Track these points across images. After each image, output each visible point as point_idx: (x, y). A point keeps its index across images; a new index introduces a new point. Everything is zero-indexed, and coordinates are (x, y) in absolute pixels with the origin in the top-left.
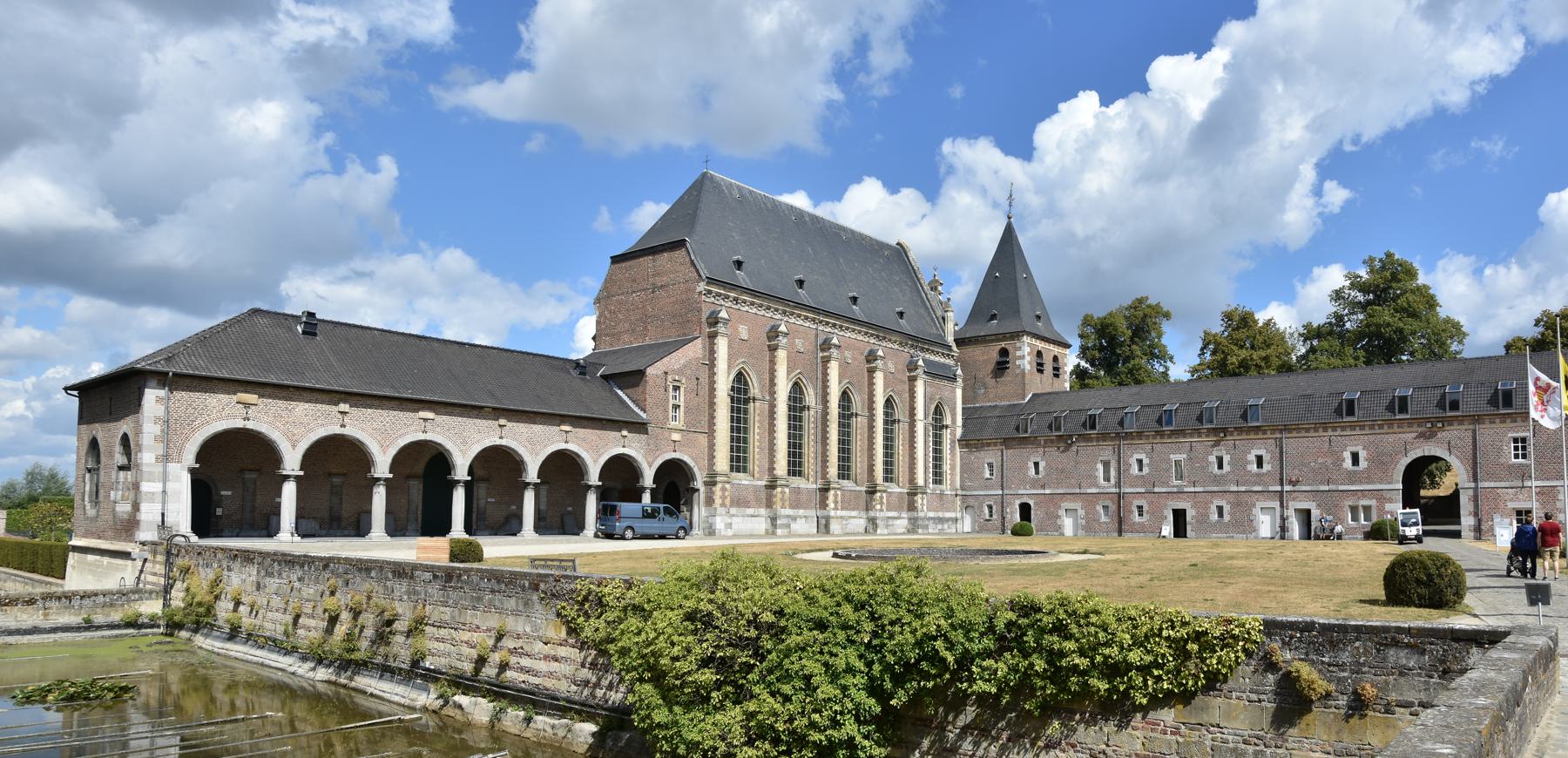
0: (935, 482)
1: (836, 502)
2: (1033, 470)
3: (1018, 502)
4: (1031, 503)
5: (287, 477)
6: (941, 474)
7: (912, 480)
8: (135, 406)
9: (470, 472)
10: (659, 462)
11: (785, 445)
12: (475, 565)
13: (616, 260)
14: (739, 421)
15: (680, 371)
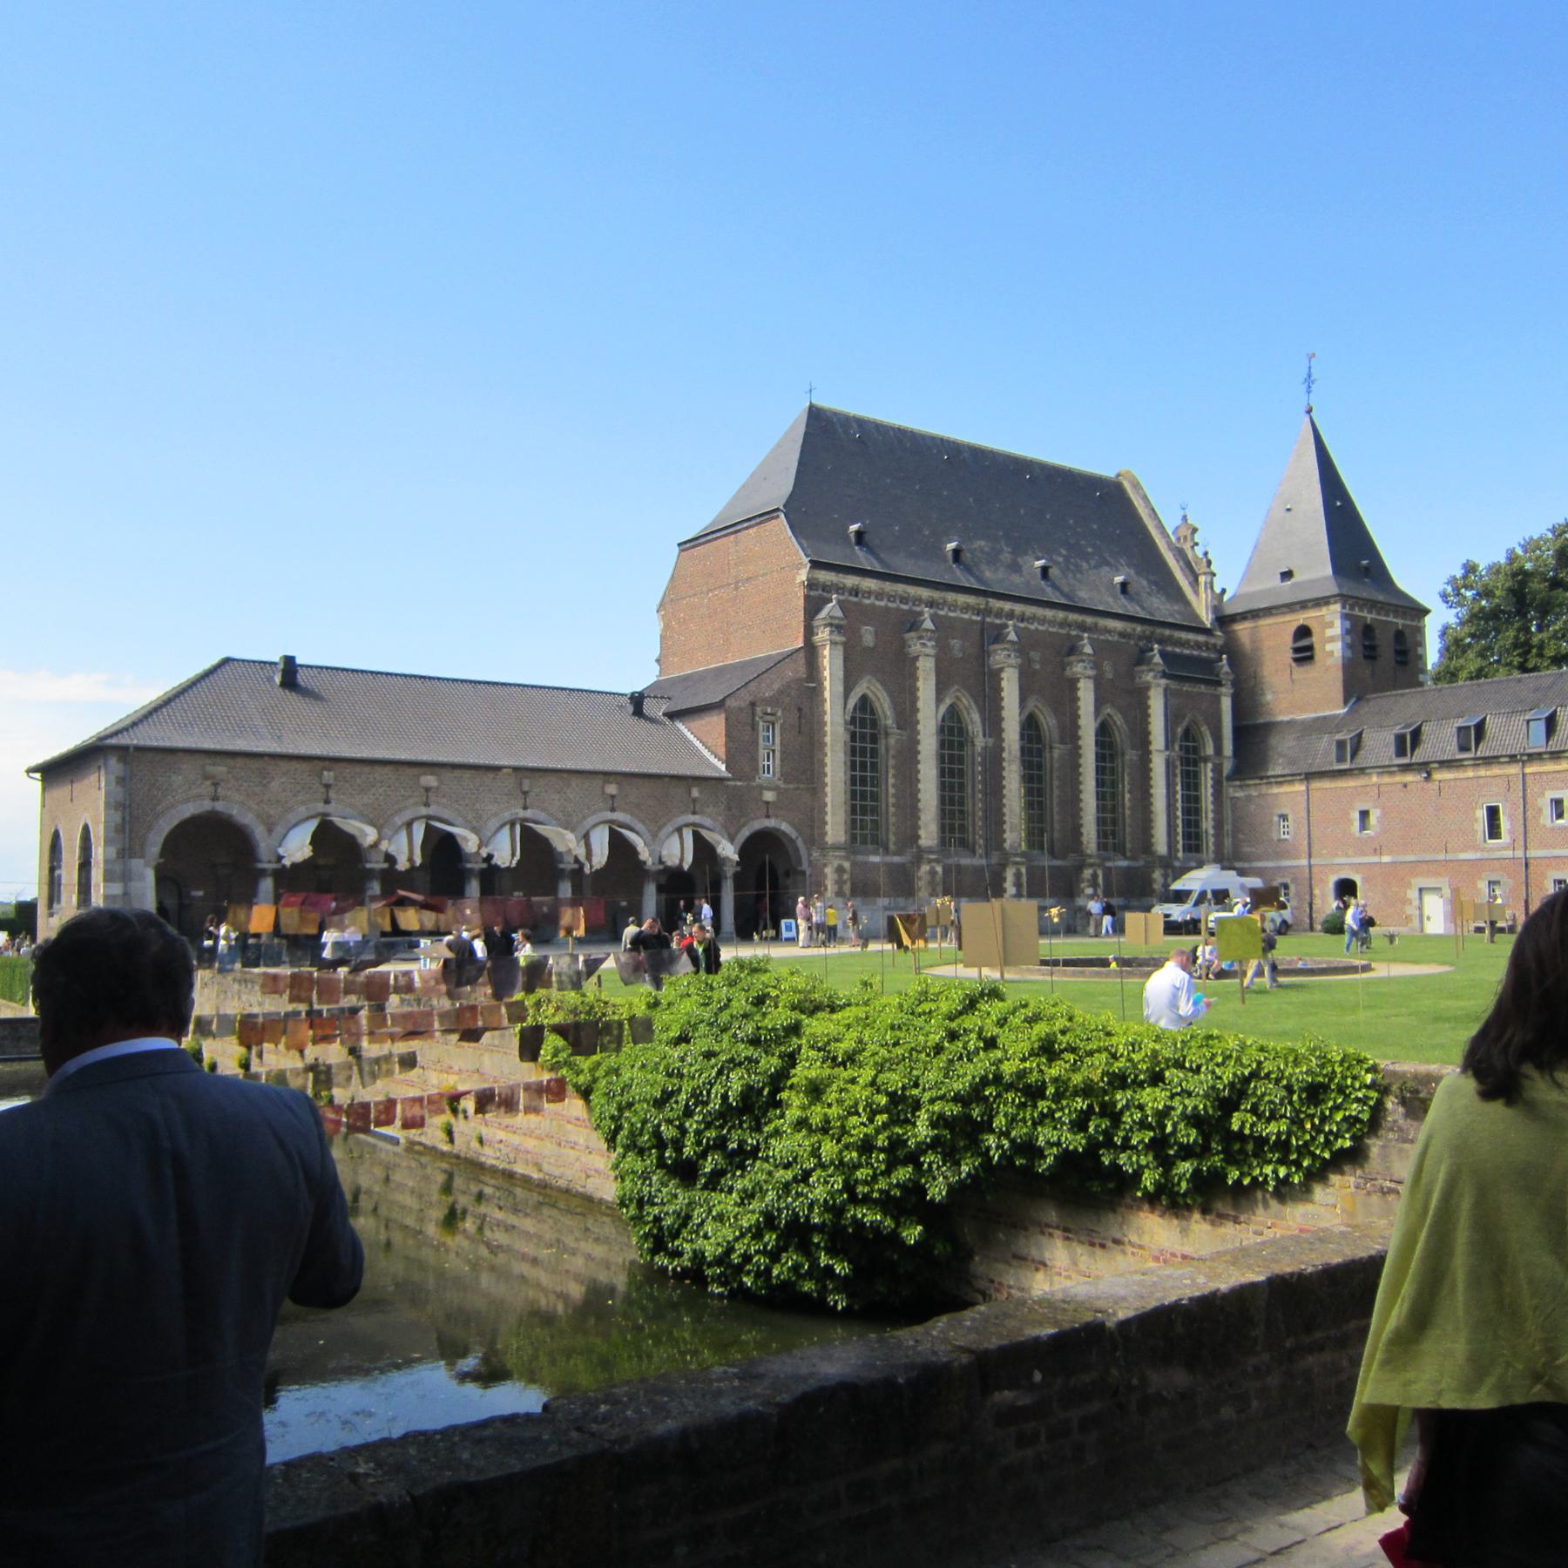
0: (1188, 848)
1: (1018, 885)
2: (1357, 824)
5: (263, 873)
6: (1198, 836)
8: (890, 941)
10: (746, 833)
13: (684, 546)
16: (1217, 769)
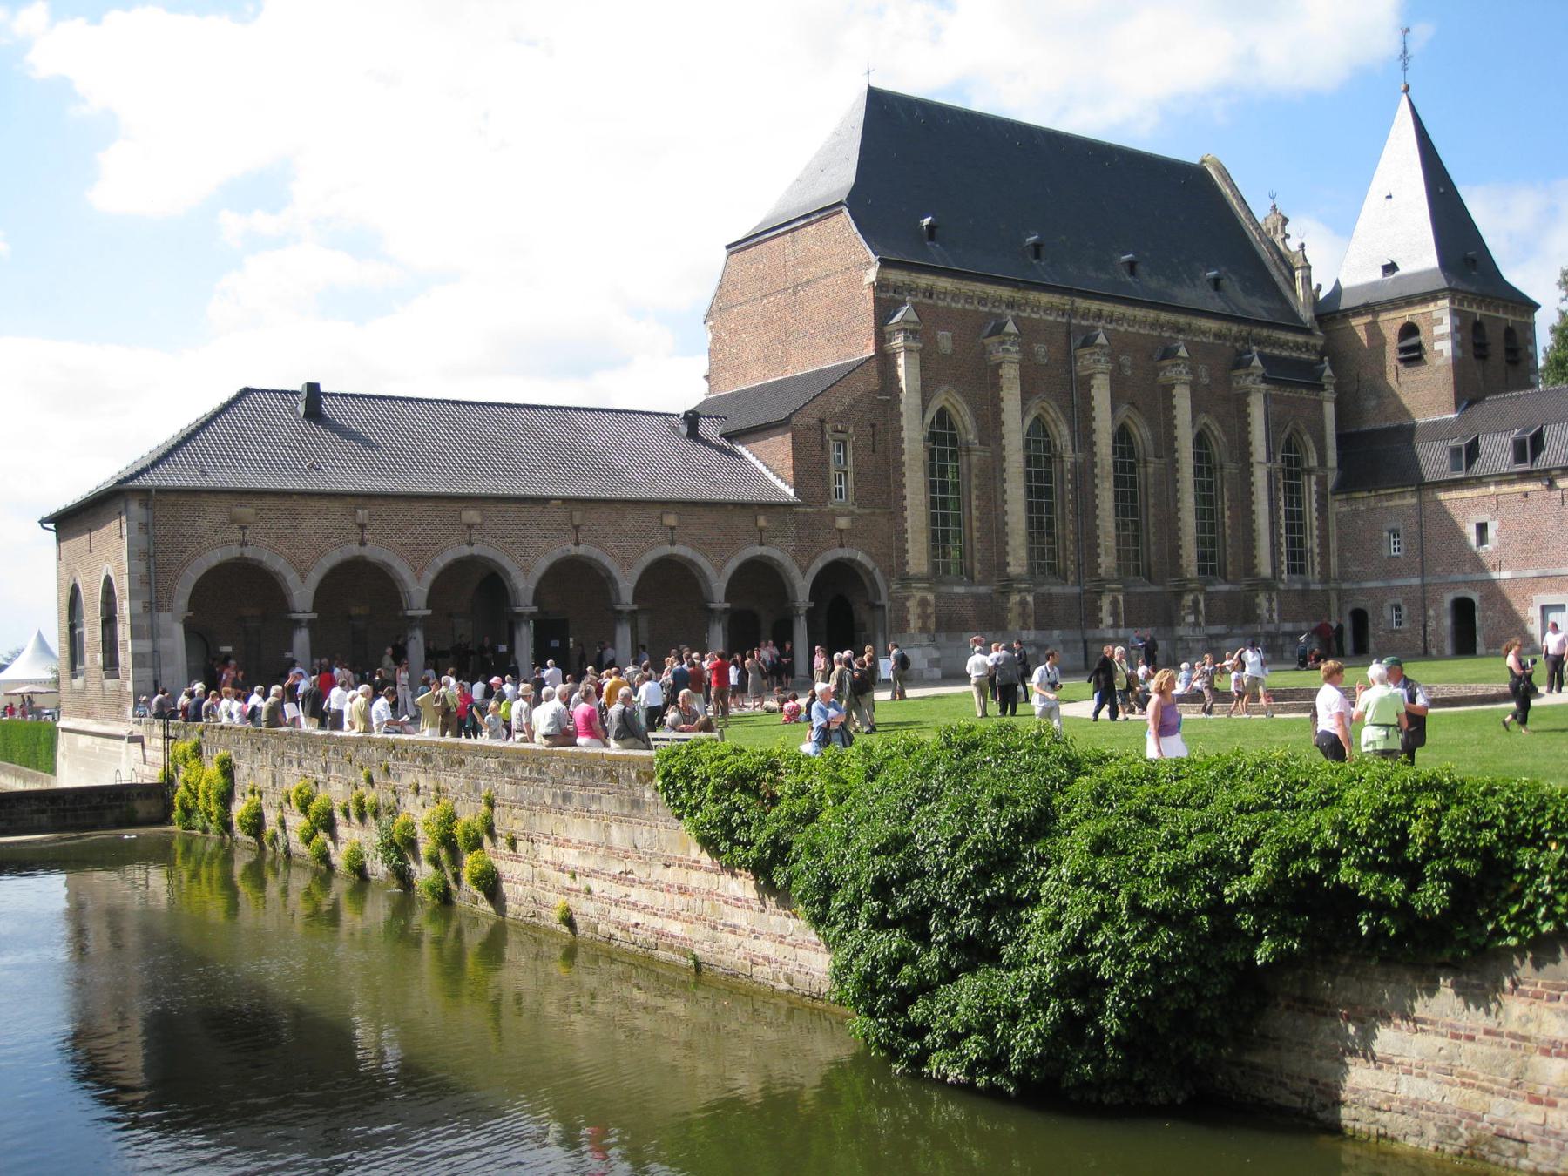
0: (1292, 570)
3: (1448, 598)
4: (1475, 597)
6: (1302, 556)
7: (1250, 568)
9: (536, 602)
10: (819, 564)
11: (1194, 556)
12: (570, 749)
13: (728, 247)
14: (1040, 510)
15: (845, 416)
16: (1322, 482)
